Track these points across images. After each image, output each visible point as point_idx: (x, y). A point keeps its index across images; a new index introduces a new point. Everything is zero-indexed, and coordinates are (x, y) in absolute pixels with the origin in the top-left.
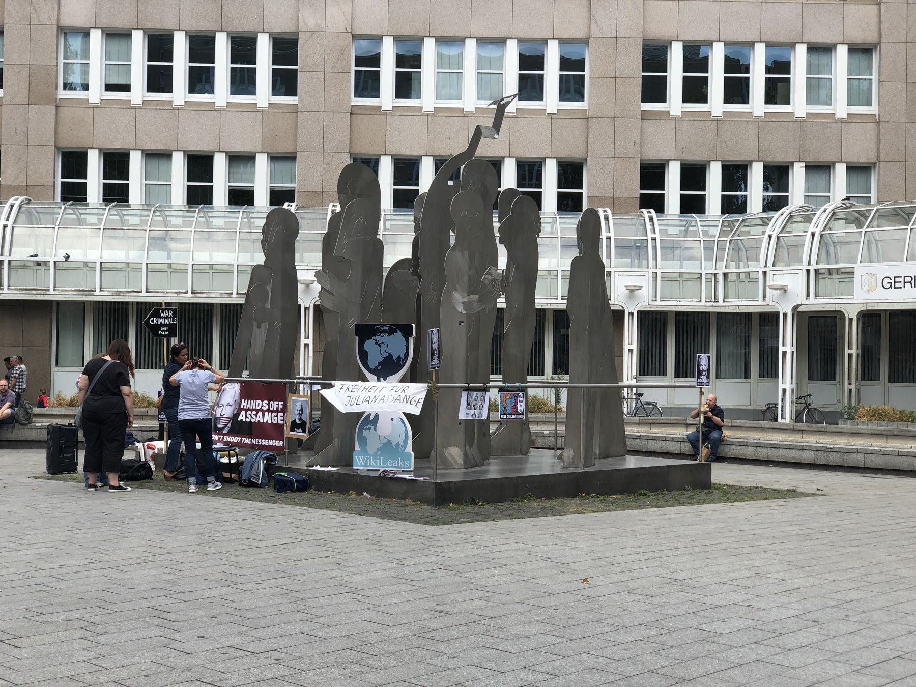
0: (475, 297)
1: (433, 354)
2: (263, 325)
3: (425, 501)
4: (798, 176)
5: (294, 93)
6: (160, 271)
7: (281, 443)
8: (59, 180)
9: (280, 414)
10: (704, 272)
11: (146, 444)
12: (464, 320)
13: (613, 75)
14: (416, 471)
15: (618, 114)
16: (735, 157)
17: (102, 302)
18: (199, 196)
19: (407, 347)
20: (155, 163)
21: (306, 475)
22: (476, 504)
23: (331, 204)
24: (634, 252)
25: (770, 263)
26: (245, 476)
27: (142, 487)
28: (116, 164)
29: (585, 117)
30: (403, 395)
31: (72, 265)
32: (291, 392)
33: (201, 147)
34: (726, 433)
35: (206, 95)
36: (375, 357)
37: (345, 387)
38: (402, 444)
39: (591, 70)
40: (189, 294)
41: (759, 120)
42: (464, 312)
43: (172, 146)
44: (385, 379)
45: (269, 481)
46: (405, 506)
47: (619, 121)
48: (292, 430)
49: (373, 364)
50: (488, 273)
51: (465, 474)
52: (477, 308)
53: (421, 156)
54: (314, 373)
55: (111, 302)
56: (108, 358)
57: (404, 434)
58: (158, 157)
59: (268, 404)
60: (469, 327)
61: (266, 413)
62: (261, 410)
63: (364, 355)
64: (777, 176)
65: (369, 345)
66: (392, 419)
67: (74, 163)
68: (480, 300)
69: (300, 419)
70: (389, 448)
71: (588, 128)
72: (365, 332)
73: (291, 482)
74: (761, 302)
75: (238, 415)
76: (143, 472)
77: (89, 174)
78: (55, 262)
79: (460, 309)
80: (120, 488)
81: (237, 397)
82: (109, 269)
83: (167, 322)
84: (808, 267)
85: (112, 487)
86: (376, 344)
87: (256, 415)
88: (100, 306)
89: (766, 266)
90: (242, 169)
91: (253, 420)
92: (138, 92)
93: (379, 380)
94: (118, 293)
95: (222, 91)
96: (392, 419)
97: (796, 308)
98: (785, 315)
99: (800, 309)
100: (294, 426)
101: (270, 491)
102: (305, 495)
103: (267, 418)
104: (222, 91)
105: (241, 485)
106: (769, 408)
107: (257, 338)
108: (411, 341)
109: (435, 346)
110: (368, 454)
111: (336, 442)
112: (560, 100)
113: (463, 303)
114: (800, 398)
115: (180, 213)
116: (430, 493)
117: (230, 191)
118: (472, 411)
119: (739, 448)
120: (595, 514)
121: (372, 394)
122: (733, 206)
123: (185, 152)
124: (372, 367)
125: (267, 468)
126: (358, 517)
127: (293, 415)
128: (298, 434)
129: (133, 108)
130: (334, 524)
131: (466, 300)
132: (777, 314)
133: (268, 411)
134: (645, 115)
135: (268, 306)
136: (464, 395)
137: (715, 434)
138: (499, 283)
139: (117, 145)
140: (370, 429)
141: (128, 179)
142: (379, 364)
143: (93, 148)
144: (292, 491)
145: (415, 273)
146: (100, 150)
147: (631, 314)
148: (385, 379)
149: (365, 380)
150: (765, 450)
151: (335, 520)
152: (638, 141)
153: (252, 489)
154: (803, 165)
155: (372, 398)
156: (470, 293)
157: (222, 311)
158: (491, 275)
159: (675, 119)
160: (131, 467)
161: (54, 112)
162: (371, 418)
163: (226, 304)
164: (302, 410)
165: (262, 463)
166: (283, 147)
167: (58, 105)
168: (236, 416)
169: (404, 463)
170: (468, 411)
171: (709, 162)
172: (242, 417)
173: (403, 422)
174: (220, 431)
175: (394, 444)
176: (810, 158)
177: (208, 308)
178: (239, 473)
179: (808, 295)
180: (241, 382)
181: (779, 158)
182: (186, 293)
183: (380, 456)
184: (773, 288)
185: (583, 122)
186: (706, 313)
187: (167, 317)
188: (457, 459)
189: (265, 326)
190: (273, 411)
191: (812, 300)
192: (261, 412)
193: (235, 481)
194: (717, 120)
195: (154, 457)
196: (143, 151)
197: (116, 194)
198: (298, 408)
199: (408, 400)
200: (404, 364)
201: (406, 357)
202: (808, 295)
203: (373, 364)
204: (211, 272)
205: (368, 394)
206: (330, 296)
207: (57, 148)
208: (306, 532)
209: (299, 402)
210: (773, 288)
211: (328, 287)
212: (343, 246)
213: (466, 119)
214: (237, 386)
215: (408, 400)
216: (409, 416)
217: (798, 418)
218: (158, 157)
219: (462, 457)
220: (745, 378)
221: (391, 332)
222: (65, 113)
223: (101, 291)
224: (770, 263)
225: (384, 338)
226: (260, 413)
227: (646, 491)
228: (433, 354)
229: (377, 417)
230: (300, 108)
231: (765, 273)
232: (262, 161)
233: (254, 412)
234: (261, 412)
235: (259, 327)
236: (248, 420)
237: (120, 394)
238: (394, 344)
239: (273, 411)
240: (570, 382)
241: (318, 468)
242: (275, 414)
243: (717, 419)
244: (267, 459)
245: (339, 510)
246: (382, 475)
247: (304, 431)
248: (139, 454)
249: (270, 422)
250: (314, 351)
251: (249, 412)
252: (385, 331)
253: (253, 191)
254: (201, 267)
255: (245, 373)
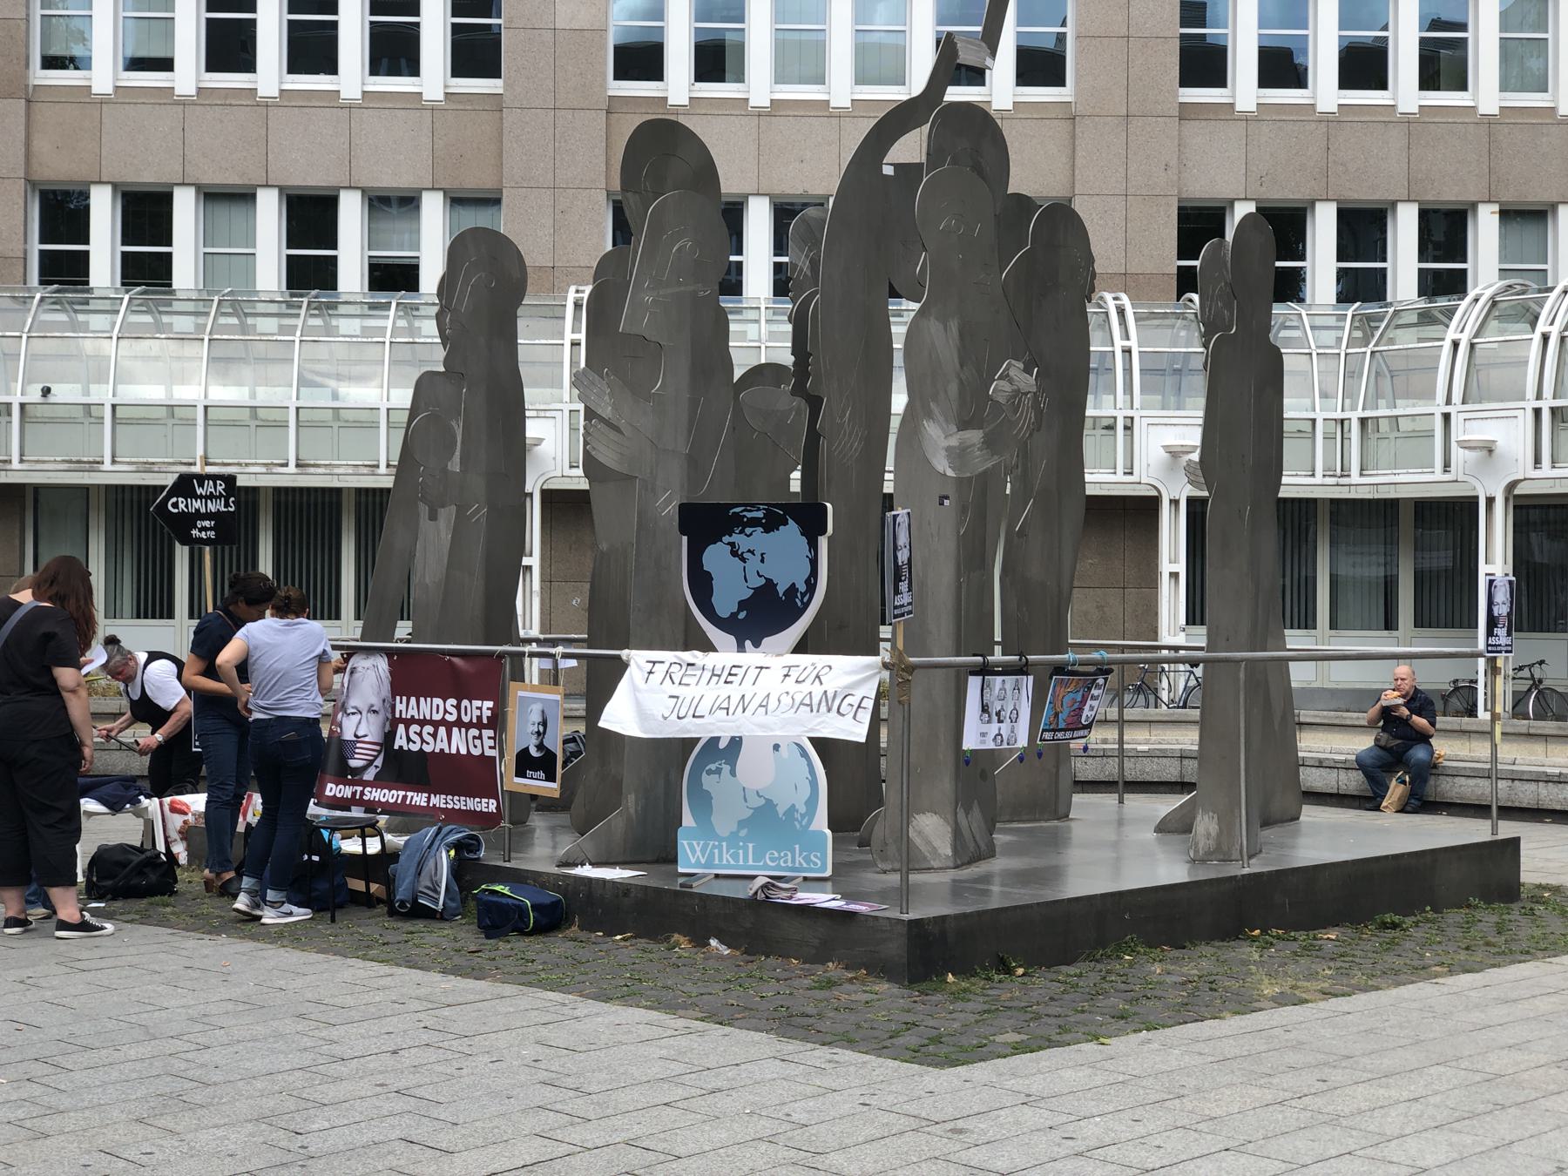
0: (974, 436)
1: (898, 579)
2: (442, 513)
3: (880, 969)
4: (1485, 230)
5: (495, 73)
6: (234, 424)
7: (492, 806)
8: (36, 247)
9: (487, 733)
10: (1320, 416)
11: (167, 800)
12: (950, 491)
13: (1124, 32)
14: (840, 878)
15: (1133, 110)
16: (1364, 194)
17: (123, 487)
18: (310, 276)
19: (814, 563)
20: (222, 211)
21: (557, 889)
22: (1009, 971)
23: (573, 289)
24: (1170, 380)
25: (1457, 395)
26: (402, 893)
27: (145, 919)
28: (146, 214)
29: (1069, 116)
30: (817, 691)
31: (61, 412)
32: (513, 679)
33: (312, 178)
34: (1443, 747)
35: (322, 77)
36: (730, 593)
37: (660, 670)
38: (803, 809)
39: (1079, 23)
40: (292, 468)
41: (1408, 121)
42: (950, 473)
43: (255, 177)
44: (757, 644)
45: (464, 901)
46: (831, 984)
47: (1136, 123)
48: (520, 773)
49: (725, 603)
50: (1003, 377)
51: (957, 889)
52: (981, 462)
53: (746, 196)
54: (545, 628)
55: (140, 487)
56: (25, 597)
57: (807, 790)
58: (225, 198)
59: (458, 707)
60: (963, 510)
61: (455, 730)
62: (443, 722)
63: (702, 584)
64: (1445, 233)
65: (716, 557)
66: (776, 747)
67: (63, 214)
68: (990, 443)
69: (540, 747)
70: (766, 820)
71: (1073, 137)
72: (705, 523)
73: (521, 910)
74: (1438, 475)
75: (390, 737)
76: (153, 877)
77: (94, 234)
78: (22, 406)
79: (942, 465)
80: (84, 926)
81: (386, 690)
82: (130, 422)
83: (212, 507)
84: (1538, 404)
85: (64, 926)
86: (734, 553)
87: (434, 736)
88: (117, 493)
89: (1448, 402)
90: (394, 225)
91: (427, 749)
92: (189, 71)
93: (741, 648)
94: (148, 468)
95: (354, 72)
96: (776, 747)
97: (1512, 485)
98: (1490, 501)
99: (1517, 492)
100: (524, 763)
101: (464, 934)
102: (558, 946)
103: (459, 743)
104: (354, 72)
105: (393, 913)
106: (1457, 689)
107: (432, 544)
108: (823, 543)
109: (903, 556)
110: (716, 837)
111: (631, 801)
112: (1018, 84)
113: (948, 449)
114: (1521, 668)
115: (273, 308)
116: (895, 948)
117: (371, 266)
118: (994, 728)
119: (1472, 782)
120: (1334, 1002)
121: (734, 691)
122: (1362, 287)
123: (281, 189)
124: (724, 611)
125: (457, 869)
126: (717, 1031)
127: (521, 734)
128: (536, 784)
129: (177, 103)
130: (656, 1070)
131: (954, 442)
132: (1473, 501)
133: (459, 723)
134: (1187, 112)
135: (455, 465)
136: (974, 683)
137: (1419, 753)
138: (1027, 401)
139: (147, 176)
140: (718, 771)
141: (170, 244)
142: (742, 605)
143: (100, 182)
144: (523, 932)
145: (799, 390)
146: (115, 186)
147: (1175, 503)
148: (757, 644)
149: (708, 647)
150: (1533, 786)
151: (654, 1051)
152: (1174, 163)
153: (420, 925)
154: (1496, 208)
155: (735, 700)
156: (963, 425)
157: (358, 504)
158: (1011, 381)
159: (1246, 118)
160: (124, 865)
161: (22, 112)
162: (722, 745)
163: (367, 490)
164: (544, 723)
165: (445, 858)
166: (475, 180)
167: (31, 98)
168: (390, 737)
169: (807, 860)
170: (985, 728)
171: (1313, 203)
172: (401, 742)
173: (804, 754)
174: (346, 774)
175: (781, 810)
176: (1511, 196)
177: (332, 496)
178: (389, 883)
179: (1537, 461)
180: (389, 653)
181: (1448, 195)
182: (286, 465)
183: (746, 840)
184: (1466, 445)
185: (1065, 126)
186: (1307, 500)
187: (211, 497)
188: (937, 843)
189: (447, 515)
190: (469, 726)
191: (1546, 470)
192: (443, 727)
193: (380, 901)
194: (1327, 119)
195: (187, 833)
196: (199, 187)
197: (147, 271)
198: (537, 718)
199: (831, 703)
200: (800, 612)
201: (811, 586)
202: (1537, 461)
203: (725, 603)
204: (336, 425)
205: (725, 690)
206: (613, 435)
207: (31, 183)
208: (579, 1105)
209: (536, 705)
210: (1466, 445)
211: (606, 411)
212: (641, 311)
213: (835, 121)
214: (382, 664)
215: (831, 703)
216: (824, 746)
217: (1518, 710)
218: (225, 198)
219: (948, 838)
220: (1387, 628)
221: (771, 523)
222: (43, 113)
223: (114, 462)
224: (1457, 395)
225: (755, 540)
226: (442, 730)
227: (1396, 919)
228: (898, 579)
229: (736, 743)
230: (507, 101)
231: (1447, 417)
232: (433, 208)
233: (429, 729)
234: (443, 727)
235: (433, 517)
236: (415, 748)
237: (53, 690)
238: (781, 555)
239: (469, 726)
240: (1211, 646)
241: (587, 871)
242: (474, 732)
243: (1420, 721)
244: (458, 846)
245: (658, 1005)
246: (761, 896)
247: (551, 777)
248: (149, 825)
249: (463, 751)
250: (542, 581)
251: (415, 728)
252: (754, 522)
253: (416, 267)
254: (317, 416)
255: (403, 629)
